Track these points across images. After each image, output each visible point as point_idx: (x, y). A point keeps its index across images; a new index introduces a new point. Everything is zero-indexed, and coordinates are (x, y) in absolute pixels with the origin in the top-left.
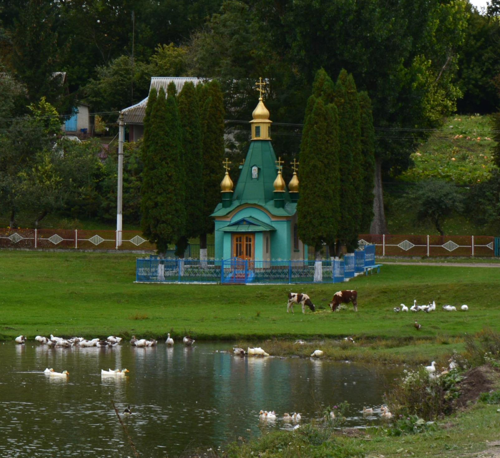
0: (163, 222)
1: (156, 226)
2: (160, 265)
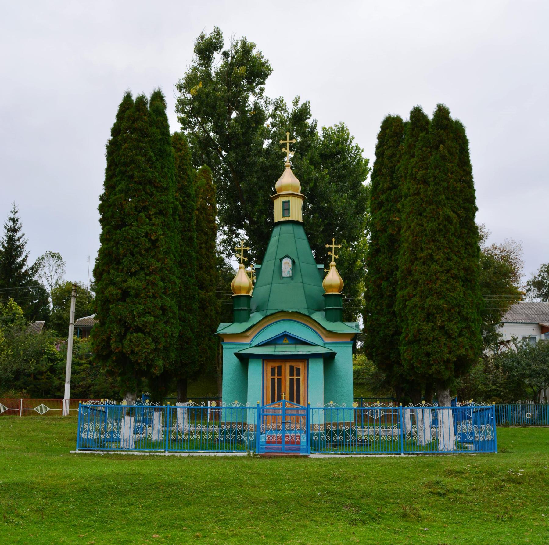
0: (138, 329)
1: (122, 337)
2: (127, 418)
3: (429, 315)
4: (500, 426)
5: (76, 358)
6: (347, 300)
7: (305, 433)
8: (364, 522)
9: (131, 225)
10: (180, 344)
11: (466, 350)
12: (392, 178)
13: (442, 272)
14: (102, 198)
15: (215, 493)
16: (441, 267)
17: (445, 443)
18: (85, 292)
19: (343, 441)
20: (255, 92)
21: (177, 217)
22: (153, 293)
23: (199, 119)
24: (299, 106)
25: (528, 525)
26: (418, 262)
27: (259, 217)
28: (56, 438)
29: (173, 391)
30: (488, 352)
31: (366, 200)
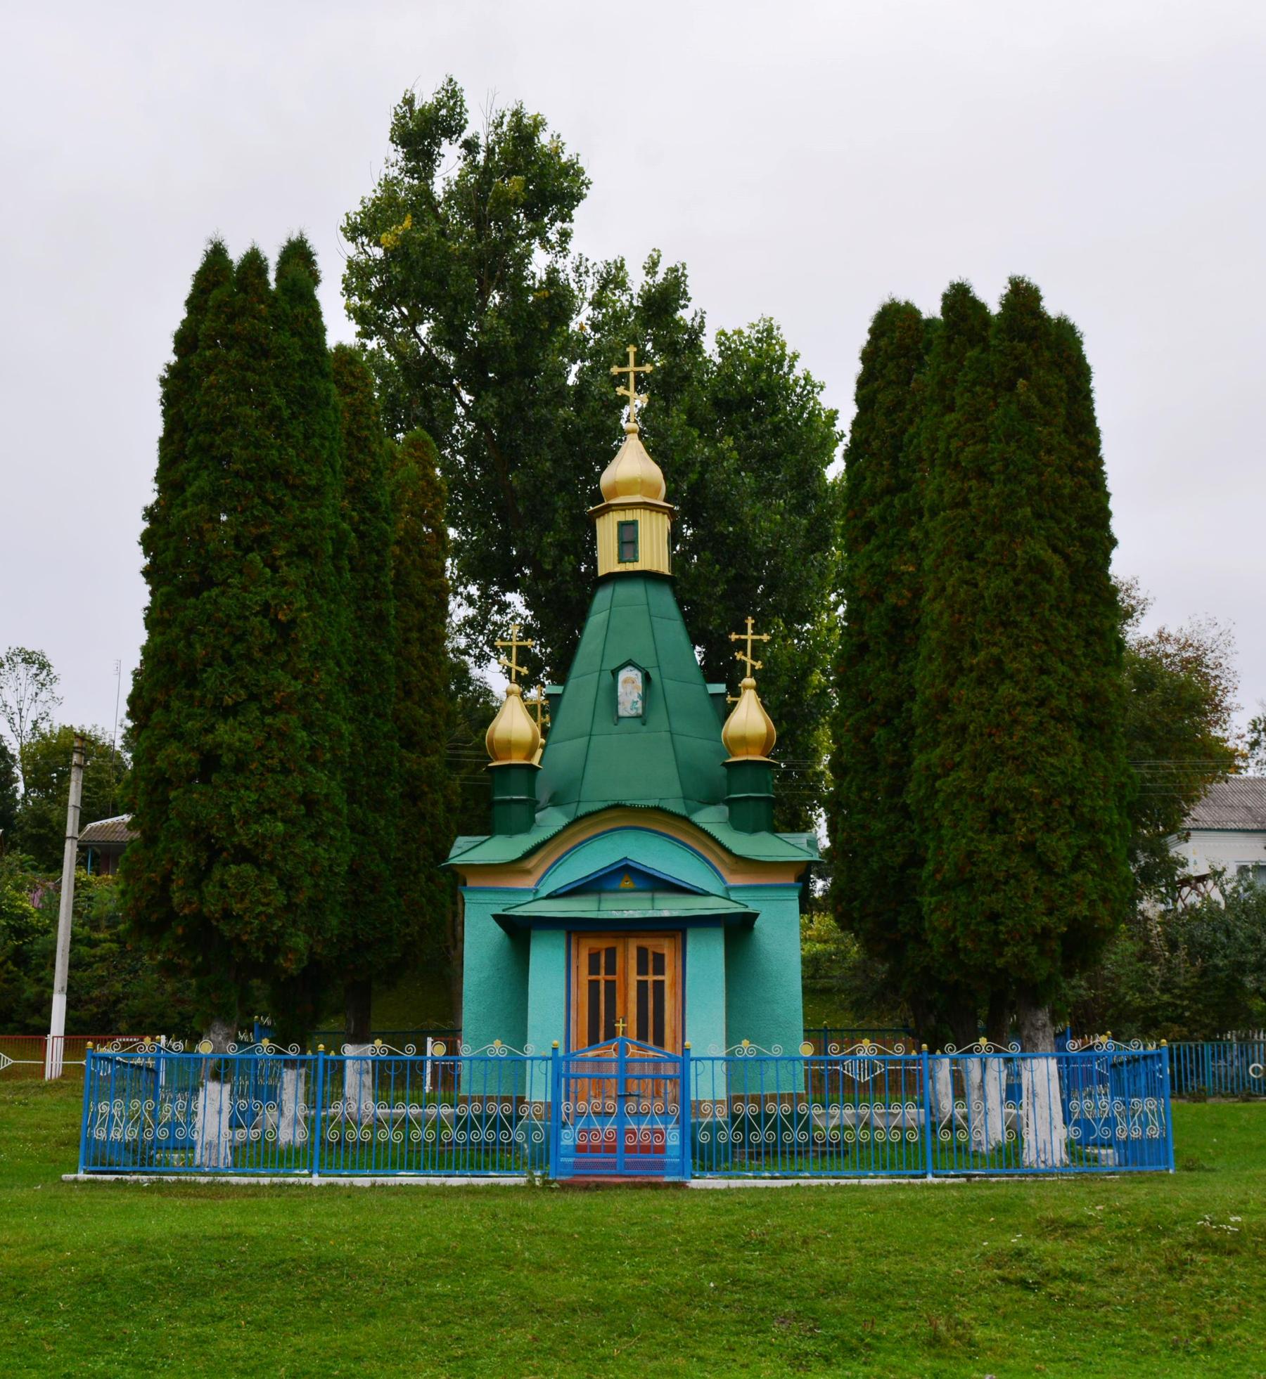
0: (243, 855)
1: (199, 875)
2: (212, 1087)
3: (994, 813)
4: (1183, 1097)
5: (83, 926)
6: (786, 775)
7: (677, 1122)
8: (827, 1359)
9: (224, 583)
10: (354, 892)
11: (1092, 904)
12: (896, 463)
13: (1028, 704)
14: (149, 514)
15: (439, 1287)
16: (1024, 690)
17: (1041, 1146)
18: (106, 752)
19: (775, 1145)
20: (549, 241)
21: (345, 563)
22: (281, 761)
23: (405, 310)
24: (659, 278)
25: (1254, 1363)
26: (965, 679)
27: (558, 561)
28: (26, 1140)
29: (336, 1012)
30: (1150, 907)
31: (832, 514)
